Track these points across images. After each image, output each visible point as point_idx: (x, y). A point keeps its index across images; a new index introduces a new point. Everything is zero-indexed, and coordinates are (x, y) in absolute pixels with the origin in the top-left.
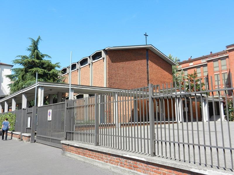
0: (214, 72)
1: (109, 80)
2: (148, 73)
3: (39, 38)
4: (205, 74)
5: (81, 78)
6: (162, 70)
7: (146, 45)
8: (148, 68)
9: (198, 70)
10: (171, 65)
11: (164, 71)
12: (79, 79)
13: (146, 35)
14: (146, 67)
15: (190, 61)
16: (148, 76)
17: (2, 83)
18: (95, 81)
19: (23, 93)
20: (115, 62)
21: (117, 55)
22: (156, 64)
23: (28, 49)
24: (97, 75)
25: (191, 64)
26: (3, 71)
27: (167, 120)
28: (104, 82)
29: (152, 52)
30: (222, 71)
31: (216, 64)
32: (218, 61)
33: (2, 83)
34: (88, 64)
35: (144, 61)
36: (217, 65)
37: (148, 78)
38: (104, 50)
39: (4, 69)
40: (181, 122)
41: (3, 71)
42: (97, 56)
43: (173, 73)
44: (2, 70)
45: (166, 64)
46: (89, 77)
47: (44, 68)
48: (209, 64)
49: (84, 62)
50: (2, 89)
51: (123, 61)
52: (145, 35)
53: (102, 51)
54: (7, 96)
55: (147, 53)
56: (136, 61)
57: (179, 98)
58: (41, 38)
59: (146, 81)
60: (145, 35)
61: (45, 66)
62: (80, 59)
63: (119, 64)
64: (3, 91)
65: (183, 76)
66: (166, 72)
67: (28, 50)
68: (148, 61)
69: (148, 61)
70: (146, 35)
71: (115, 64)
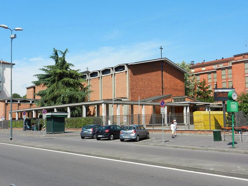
0: (222, 80)
1: (131, 90)
2: (163, 83)
3: (67, 50)
4: (215, 80)
5: (103, 85)
6: (175, 79)
7: (162, 58)
8: (162, 79)
9: (210, 76)
10: (184, 73)
11: (177, 80)
12: (100, 86)
13: (161, 48)
14: (161, 77)
15: (203, 65)
16: (163, 85)
17: (4, 84)
18: (117, 90)
19: (83, 105)
20: (136, 75)
21: (137, 69)
22: (169, 73)
23: (51, 57)
24: (121, 85)
25: (204, 69)
26: (5, 70)
27: (41, 134)
28: (126, 91)
29: (167, 63)
30: (228, 79)
31: (224, 72)
32: (225, 69)
33: (4, 84)
34: (110, 74)
35: (160, 72)
36: (225, 74)
37: (163, 87)
38: (127, 65)
39: (6, 68)
40: (188, 124)
41: (5, 70)
42: (120, 68)
43: (185, 80)
44: (4, 69)
45: (178, 72)
46: (112, 85)
47: (74, 78)
48: (218, 71)
49: (106, 71)
50: (4, 89)
51: (142, 74)
52: (160, 48)
53: (125, 65)
54: (21, 98)
55: (162, 65)
56: (152, 73)
57: (187, 107)
58: (68, 50)
59: (161, 89)
60: (160, 48)
61: (74, 76)
62: (102, 68)
63: (139, 76)
64: (6, 92)
65: (194, 81)
66: (178, 80)
67: (50, 57)
68: (162, 72)
69: (162, 72)
70: (161, 48)
71: (135, 76)
